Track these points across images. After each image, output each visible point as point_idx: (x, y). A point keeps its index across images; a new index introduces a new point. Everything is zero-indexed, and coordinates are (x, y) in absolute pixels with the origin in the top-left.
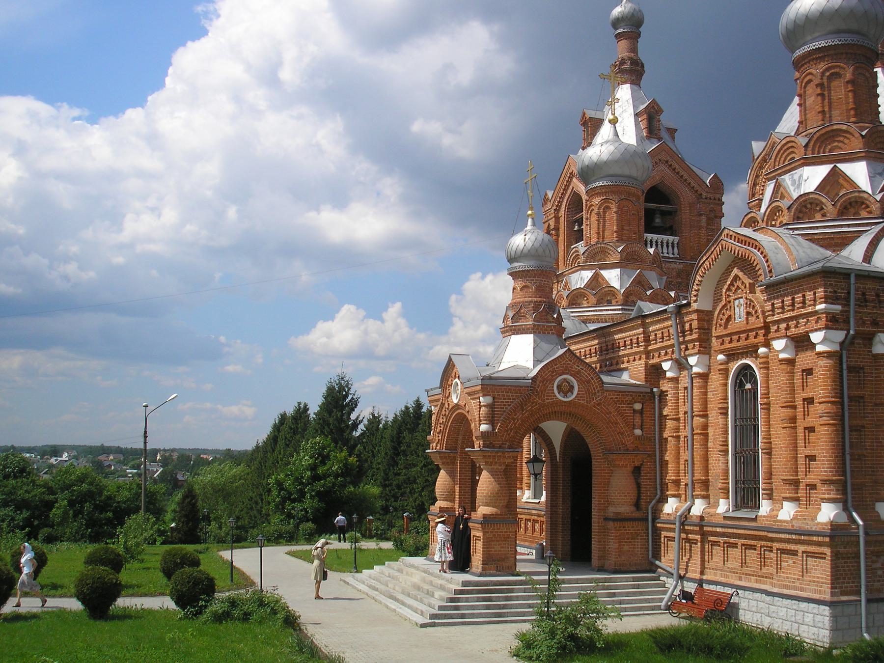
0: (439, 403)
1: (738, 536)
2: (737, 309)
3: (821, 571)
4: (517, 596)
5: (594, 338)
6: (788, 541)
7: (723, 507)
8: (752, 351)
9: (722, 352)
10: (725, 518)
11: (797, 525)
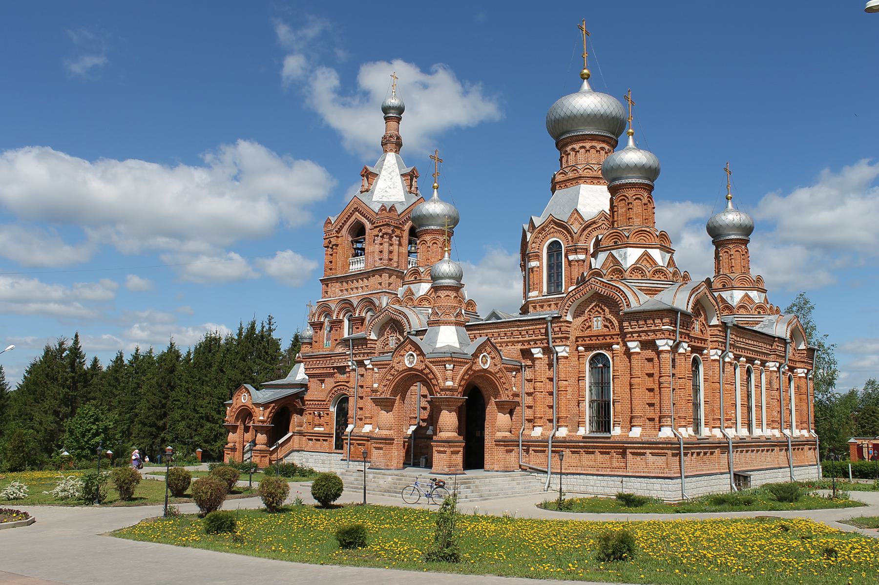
1: (597, 447)
3: (812, 455)
4: (757, 401)
7: (583, 431)
8: (609, 347)
9: (582, 345)
10: (584, 438)
11: (645, 439)
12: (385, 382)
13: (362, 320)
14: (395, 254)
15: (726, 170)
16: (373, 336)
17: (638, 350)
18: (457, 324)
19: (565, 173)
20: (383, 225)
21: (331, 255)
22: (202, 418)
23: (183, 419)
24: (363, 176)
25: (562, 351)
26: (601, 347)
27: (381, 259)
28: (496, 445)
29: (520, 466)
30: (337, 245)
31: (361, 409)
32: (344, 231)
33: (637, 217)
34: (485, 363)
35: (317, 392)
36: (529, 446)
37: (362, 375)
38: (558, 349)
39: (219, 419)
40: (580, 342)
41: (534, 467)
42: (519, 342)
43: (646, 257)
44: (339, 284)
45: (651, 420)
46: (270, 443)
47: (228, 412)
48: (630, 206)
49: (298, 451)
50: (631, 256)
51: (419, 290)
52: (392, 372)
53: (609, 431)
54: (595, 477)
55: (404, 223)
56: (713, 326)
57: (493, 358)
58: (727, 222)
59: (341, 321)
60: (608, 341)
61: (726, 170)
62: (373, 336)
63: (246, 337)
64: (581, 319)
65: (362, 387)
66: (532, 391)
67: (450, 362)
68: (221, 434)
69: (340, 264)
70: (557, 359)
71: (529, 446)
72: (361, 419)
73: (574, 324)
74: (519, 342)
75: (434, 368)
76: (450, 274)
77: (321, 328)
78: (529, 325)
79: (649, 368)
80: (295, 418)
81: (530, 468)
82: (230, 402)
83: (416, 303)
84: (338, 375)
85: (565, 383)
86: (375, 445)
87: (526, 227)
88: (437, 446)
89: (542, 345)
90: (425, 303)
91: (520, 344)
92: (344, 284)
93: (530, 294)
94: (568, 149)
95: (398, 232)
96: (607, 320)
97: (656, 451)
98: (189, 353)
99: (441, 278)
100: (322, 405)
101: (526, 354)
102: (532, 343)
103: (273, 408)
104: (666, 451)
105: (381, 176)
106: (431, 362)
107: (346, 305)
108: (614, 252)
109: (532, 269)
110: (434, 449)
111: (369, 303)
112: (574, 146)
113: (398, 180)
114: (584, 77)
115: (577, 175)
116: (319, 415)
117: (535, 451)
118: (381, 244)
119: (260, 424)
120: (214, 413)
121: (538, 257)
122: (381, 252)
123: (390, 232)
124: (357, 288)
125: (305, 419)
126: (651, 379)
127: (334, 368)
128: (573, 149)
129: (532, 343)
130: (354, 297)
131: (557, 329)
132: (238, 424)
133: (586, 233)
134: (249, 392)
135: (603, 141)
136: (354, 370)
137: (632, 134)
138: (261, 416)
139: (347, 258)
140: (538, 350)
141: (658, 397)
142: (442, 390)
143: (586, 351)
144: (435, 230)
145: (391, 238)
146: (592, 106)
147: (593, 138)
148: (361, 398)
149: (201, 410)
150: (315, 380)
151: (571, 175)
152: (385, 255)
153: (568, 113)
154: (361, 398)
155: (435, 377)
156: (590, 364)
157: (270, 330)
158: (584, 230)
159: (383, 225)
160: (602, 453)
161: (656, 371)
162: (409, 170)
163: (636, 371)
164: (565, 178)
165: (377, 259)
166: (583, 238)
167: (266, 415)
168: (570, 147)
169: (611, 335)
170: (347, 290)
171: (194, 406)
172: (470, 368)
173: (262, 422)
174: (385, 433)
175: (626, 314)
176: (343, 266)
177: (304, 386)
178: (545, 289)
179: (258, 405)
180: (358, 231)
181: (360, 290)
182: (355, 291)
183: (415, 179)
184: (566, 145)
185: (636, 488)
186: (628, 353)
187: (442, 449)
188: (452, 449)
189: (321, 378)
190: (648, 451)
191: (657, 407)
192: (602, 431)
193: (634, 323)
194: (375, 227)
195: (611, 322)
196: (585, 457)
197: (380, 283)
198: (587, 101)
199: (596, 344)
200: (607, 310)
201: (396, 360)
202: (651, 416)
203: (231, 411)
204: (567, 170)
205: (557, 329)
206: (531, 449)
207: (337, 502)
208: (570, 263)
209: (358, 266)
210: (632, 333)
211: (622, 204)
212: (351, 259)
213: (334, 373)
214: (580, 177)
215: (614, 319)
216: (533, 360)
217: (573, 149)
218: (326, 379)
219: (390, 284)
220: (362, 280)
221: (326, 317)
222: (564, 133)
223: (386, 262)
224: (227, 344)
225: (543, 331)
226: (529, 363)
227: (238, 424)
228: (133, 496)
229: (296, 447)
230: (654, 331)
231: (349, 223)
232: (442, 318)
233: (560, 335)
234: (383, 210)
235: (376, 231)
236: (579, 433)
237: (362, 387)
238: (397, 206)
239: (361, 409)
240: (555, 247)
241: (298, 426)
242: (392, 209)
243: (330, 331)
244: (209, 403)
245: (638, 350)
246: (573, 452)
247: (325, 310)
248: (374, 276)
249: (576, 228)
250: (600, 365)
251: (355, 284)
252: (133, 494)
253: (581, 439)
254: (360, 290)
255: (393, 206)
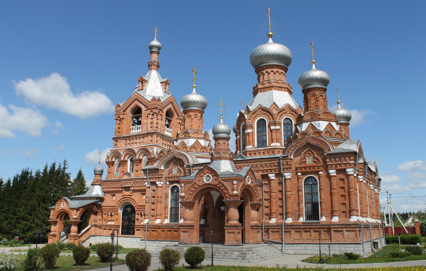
0: (192, 183)
2: (308, 160)
5: (277, 160)
6: (339, 228)
8: (317, 173)
9: (300, 172)
10: (303, 223)
12: (189, 192)
13: (141, 160)
14: (159, 124)
15: (242, 102)
16: (162, 168)
17: (335, 174)
18: (231, 159)
19: (263, 84)
20: (154, 108)
21: (119, 124)
22: (19, 218)
23: (6, 219)
24: (139, 81)
25: (288, 175)
26: (311, 173)
27: (152, 127)
28: (251, 229)
29: (263, 240)
30: (123, 119)
31: (153, 210)
32: (128, 111)
33: (321, 105)
34: (248, 181)
35: (110, 201)
36: (268, 229)
37: (154, 190)
38: (285, 174)
39: (31, 218)
40: (299, 171)
41: (273, 241)
42: (261, 170)
43: (197, 143)
44: (124, 141)
45: (343, 212)
46: (79, 231)
47: (51, 213)
48: (318, 99)
49: (94, 236)
50: (190, 142)
51: (189, 143)
52: (195, 186)
53: (318, 220)
54: (312, 245)
55: (164, 108)
56: (360, 163)
57: (251, 179)
58: (340, 114)
59: (126, 161)
60: (316, 169)
61: (242, 102)
62: (162, 168)
63: (50, 172)
64: (299, 158)
65: (154, 197)
66: (268, 198)
67: (236, 180)
68: (32, 227)
69: (125, 129)
70: (285, 179)
71: (268, 229)
72: (153, 216)
73: (295, 160)
74: (261, 170)
75: (225, 184)
76: (226, 131)
77: (113, 165)
78: (267, 161)
79: (341, 184)
80: (93, 217)
81: (269, 241)
82: (54, 207)
83: (188, 149)
84: (124, 192)
85: (290, 193)
86: (182, 230)
87: (243, 111)
88: (228, 229)
89: (275, 172)
90: (194, 150)
91: (261, 172)
92: (128, 140)
93: (247, 147)
94: (264, 72)
95: (161, 113)
96: (315, 158)
97: (349, 229)
98: (9, 181)
99: (221, 133)
100: (113, 209)
101: (265, 177)
102: (269, 171)
103: (82, 211)
104: (356, 229)
105: (150, 82)
106: (223, 180)
107: (131, 152)
108: (312, 122)
109: (248, 133)
110: (226, 231)
111: (145, 151)
112: (268, 70)
113: (159, 85)
114: (270, 36)
115: (271, 85)
116: (111, 215)
117: (272, 232)
118: (152, 119)
119: (74, 220)
120: (27, 215)
121: (252, 127)
122: (152, 123)
123: (158, 112)
124: (136, 143)
125: (99, 217)
126: (343, 190)
127: (122, 188)
128: (267, 72)
129: (269, 171)
130: (136, 147)
131: (285, 163)
132: (58, 220)
133: (280, 114)
134: (68, 203)
135: (282, 69)
136: (149, 187)
137: (314, 63)
138: (75, 216)
139: (129, 126)
140: (273, 175)
141: (347, 200)
142: (231, 196)
143: (302, 175)
144: (196, 110)
145: (157, 115)
146: (279, 50)
147: (278, 67)
148: (153, 203)
149: (19, 214)
150: (109, 195)
151: (267, 85)
152: (155, 125)
153: (266, 53)
154: (153, 203)
155: (226, 189)
156: (305, 182)
157: (64, 168)
158: (279, 113)
159: (154, 108)
160: (314, 231)
161: (346, 186)
162: (165, 80)
163: (334, 186)
164: (264, 86)
165: (149, 126)
166: (278, 118)
167: (78, 215)
168: (265, 71)
169: (318, 166)
170: (129, 144)
171: (14, 211)
172: (244, 184)
173: (76, 219)
174: (189, 222)
175: (328, 154)
176: (127, 130)
177: (102, 199)
178: (256, 145)
179: (73, 209)
180: (137, 112)
181: (138, 144)
182: (135, 144)
183: (167, 85)
184: (263, 69)
185: (351, 249)
186: (329, 177)
187: (231, 231)
188: (238, 231)
189: (113, 194)
190: (344, 229)
191: (348, 205)
192: (314, 219)
193: (332, 160)
194: (148, 109)
195: (317, 159)
196: (304, 234)
197: (152, 141)
198: (273, 48)
199: (309, 171)
200: (315, 153)
201: (197, 179)
202: (344, 210)
203: (54, 213)
204: (265, 82)
205: (285, 163)
206: (270, 230)
207: (198, 265)
208: (271, 131)
209: (135, 131)
210: (331, 165)
211: (313, 98)
212: (131, 127)
213: (122, 191)
214: (272, 86)
215: (319, 158)
216: (270, 181)
217: (267, 72)
218: (117, 194)
219: (157, 141)
220: (139, 138)
221: (116, 158)
222: (260, 65)
223: (155, 129)
224: (36, 175)
225: (276, 164)
226: (266, 182)
227: (58, 220)
228: (55, 266)
229: (93, 234)
230: (345, 164)
231: (131, 107)
232: (222, 155)
233: (287, 167)
234: (153, 100)
235: (149, 112)
236: (300, 221)
237: (154, 197)
238: (161, 98)
239: (153, 210)
240: (261, 123)
241: (94, 222)
242: (159, 100)
243: (119, 167)
244: (24, 210)
245: (335, 174)
246: (296, 232)
247: (116, 154)
248: (147, 136)
249: (275, 112)
250: (311, 183)
251: (135, 141)
252: (54, 264)
253: (301, 224)
254: (138, 144)
255: (159, 98)
